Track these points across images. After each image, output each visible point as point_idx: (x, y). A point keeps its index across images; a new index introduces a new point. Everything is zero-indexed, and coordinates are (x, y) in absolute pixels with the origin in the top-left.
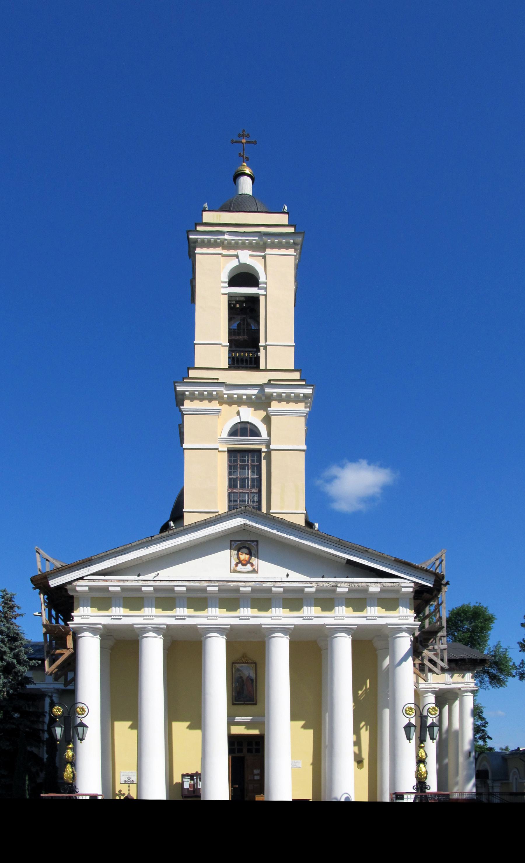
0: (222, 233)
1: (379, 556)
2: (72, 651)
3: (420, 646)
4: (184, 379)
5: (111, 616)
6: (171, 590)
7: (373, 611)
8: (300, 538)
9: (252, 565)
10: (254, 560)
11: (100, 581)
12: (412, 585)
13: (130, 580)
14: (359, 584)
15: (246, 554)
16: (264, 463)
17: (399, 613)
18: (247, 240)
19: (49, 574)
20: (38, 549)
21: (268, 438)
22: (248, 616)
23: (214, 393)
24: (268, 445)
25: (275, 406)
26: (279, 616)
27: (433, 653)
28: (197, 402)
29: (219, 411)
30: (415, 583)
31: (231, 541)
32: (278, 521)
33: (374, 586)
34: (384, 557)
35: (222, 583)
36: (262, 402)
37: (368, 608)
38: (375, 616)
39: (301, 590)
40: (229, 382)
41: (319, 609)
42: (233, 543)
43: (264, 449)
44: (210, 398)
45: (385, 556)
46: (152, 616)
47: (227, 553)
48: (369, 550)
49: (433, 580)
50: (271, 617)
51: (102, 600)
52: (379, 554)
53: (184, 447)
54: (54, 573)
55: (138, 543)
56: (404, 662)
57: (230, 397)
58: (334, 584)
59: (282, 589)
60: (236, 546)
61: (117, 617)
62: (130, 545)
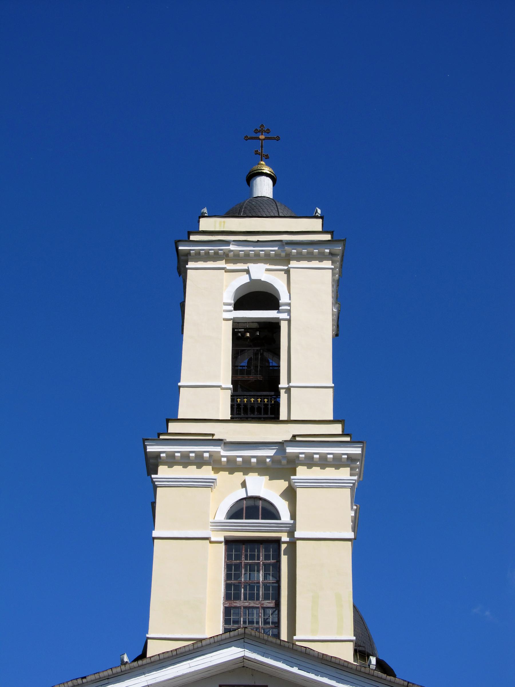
0: (227, 243)
16: (284, 559)
18: (262, 251)
21: (292, 522)
28: (192, 468)
40: (229, 439)
43: (285, 538)
44: (199, 461)
57: (231, 460)
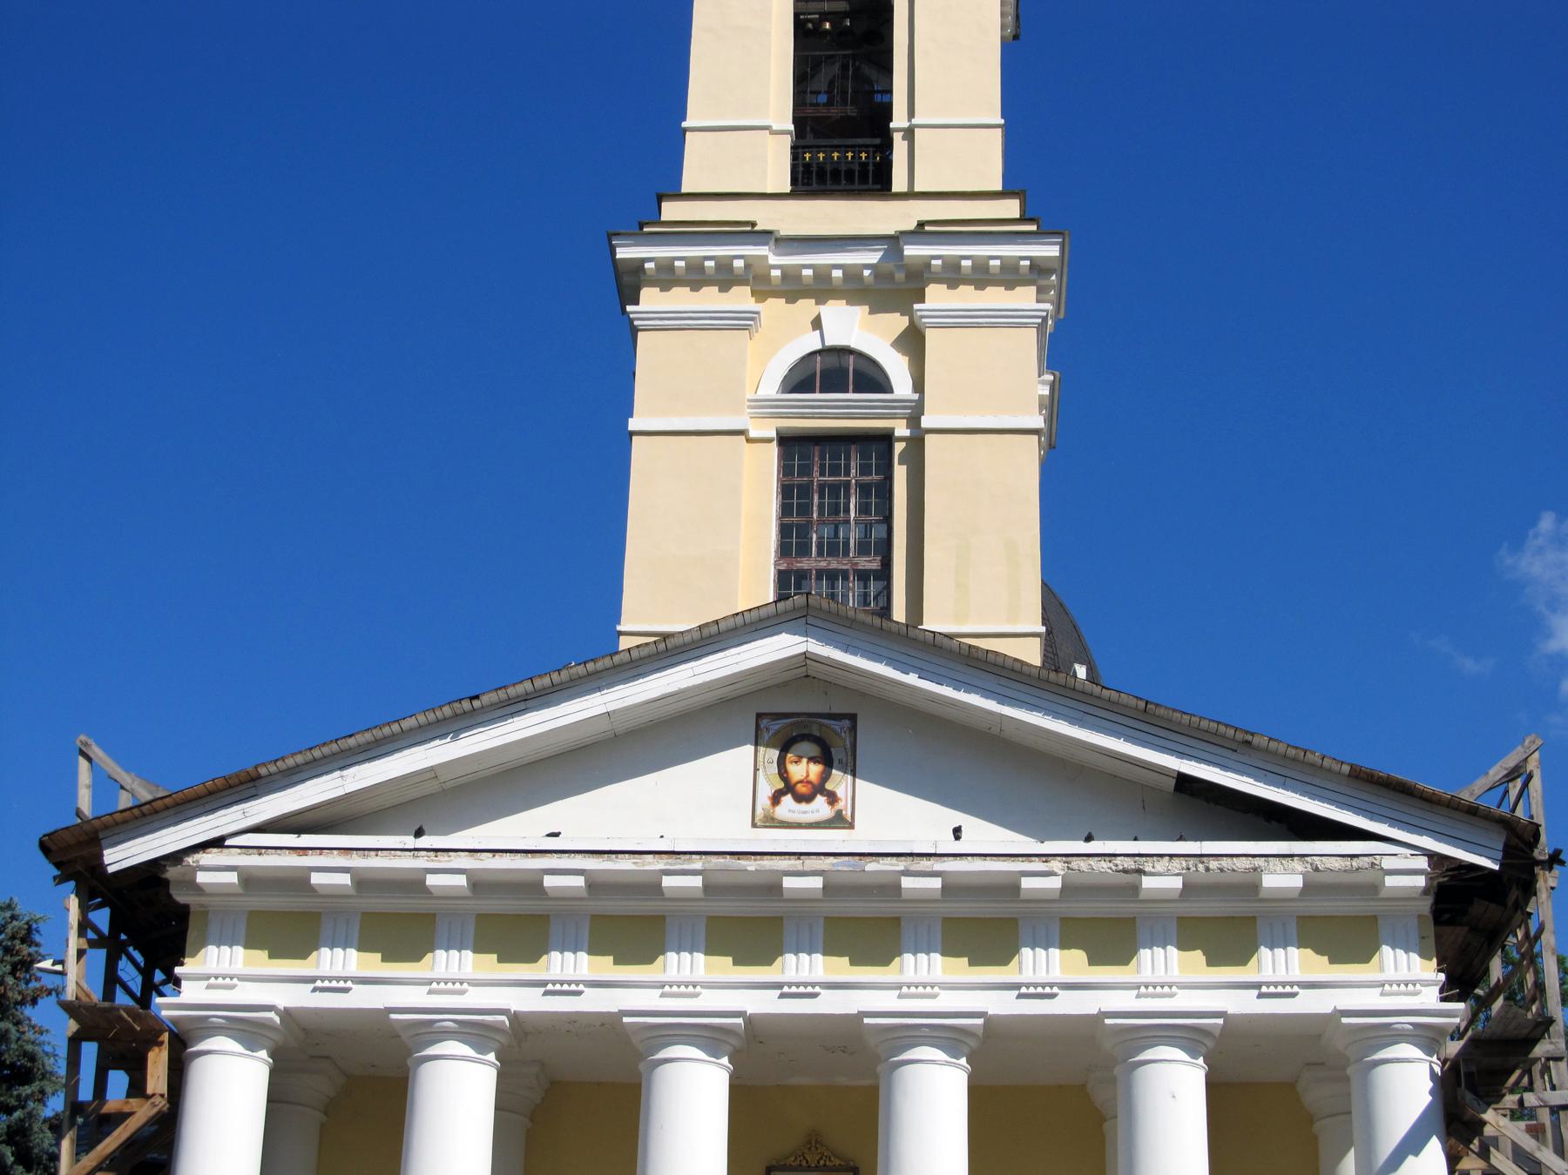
1: (1294, 760)
2: (162, 1104)
3: (1469, 1096)
4: (641, 227)
5: (312, 980)
6: (530, 886)
7: (1282, 963)
8: (1003, 699)
9: (832, 798)
10: (840, 782)
11: (281, 855)
12: (1422, 863)
13: (389, 853)
14: (1225, 863)
15: (811, 759)
16: (900, 473)
17: (1382, 969)
19: (106, 827)
20: (86, 744)
21: (916, 396)
22: (814, 985)
23: (739, 264)
24: (914, 420)
25: (937, 297)
26: (932, 982)
27: (1522, 1124)
29: (753, 316)
30: (1433, 857)
31: (759, 716)
32: (925, 643)
33: (1279, 868)
34: (1313, 765)
35: (714, 859)
36: (895, 285)
37: (1264, 951)
38: (1290, 982)
39: (1008, 888)
40: (785, 230)
41: (1079, 955)
42: (764, 722)
43: (902, 430)
44: (725, 277)
45: (1314, 758)
46: (462, 980)
47: (742, 756)
48: (1256, 740)
49: (1500, 847)
50: (899, 986)
51: (287, 920)
52: (1292, 752)
53: (631, 428)
54: (125, 822)
55: (422, 719)
56: (1411, 1158)
57: (790, 275)
58: (1129, 864)
59: (936, 883)
60: (776, 733)
61: (334, 984)
62: (395, 727)
